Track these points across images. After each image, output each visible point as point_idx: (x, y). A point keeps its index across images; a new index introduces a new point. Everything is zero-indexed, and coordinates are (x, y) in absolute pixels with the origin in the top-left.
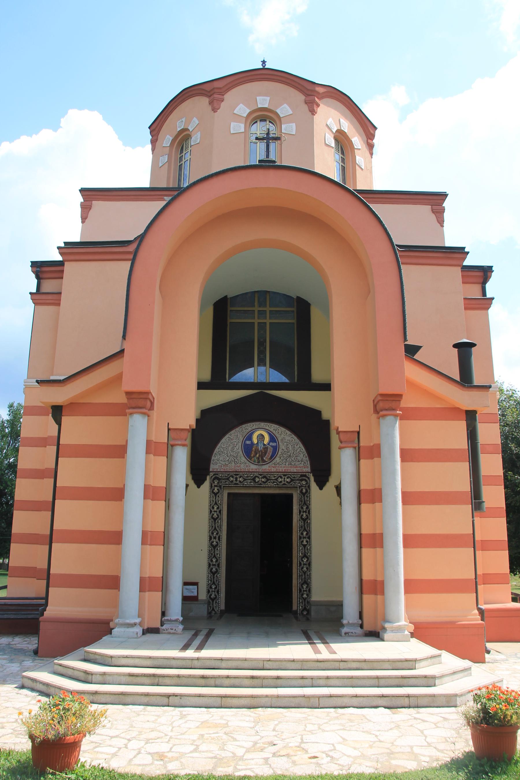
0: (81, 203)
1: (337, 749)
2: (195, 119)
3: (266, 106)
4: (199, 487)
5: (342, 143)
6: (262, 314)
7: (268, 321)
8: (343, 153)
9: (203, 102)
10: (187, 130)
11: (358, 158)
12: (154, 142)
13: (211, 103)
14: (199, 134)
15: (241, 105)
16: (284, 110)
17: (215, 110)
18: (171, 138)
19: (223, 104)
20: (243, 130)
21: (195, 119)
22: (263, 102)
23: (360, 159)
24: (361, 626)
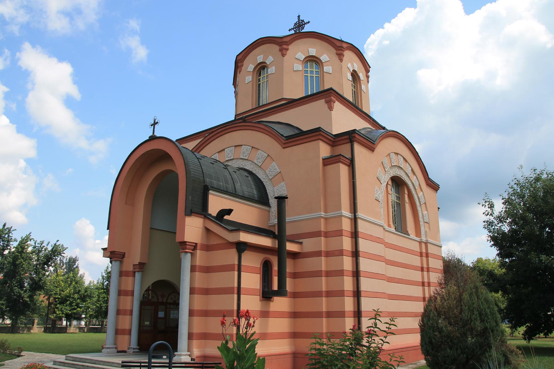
1: (418, 243)
2: (270, 57)
3: (314, 55)
5: (354, 75)
6: (312, 72)
7: (314, 75)
10: (265, 63)
11: (362, 86)
13: (281, 50)
16: (324, 58)
17: (283, 55)
18: (253, 67)
19: (288, 52)
21: (270, 57)
22: (313, 52)
24: (116, 348)
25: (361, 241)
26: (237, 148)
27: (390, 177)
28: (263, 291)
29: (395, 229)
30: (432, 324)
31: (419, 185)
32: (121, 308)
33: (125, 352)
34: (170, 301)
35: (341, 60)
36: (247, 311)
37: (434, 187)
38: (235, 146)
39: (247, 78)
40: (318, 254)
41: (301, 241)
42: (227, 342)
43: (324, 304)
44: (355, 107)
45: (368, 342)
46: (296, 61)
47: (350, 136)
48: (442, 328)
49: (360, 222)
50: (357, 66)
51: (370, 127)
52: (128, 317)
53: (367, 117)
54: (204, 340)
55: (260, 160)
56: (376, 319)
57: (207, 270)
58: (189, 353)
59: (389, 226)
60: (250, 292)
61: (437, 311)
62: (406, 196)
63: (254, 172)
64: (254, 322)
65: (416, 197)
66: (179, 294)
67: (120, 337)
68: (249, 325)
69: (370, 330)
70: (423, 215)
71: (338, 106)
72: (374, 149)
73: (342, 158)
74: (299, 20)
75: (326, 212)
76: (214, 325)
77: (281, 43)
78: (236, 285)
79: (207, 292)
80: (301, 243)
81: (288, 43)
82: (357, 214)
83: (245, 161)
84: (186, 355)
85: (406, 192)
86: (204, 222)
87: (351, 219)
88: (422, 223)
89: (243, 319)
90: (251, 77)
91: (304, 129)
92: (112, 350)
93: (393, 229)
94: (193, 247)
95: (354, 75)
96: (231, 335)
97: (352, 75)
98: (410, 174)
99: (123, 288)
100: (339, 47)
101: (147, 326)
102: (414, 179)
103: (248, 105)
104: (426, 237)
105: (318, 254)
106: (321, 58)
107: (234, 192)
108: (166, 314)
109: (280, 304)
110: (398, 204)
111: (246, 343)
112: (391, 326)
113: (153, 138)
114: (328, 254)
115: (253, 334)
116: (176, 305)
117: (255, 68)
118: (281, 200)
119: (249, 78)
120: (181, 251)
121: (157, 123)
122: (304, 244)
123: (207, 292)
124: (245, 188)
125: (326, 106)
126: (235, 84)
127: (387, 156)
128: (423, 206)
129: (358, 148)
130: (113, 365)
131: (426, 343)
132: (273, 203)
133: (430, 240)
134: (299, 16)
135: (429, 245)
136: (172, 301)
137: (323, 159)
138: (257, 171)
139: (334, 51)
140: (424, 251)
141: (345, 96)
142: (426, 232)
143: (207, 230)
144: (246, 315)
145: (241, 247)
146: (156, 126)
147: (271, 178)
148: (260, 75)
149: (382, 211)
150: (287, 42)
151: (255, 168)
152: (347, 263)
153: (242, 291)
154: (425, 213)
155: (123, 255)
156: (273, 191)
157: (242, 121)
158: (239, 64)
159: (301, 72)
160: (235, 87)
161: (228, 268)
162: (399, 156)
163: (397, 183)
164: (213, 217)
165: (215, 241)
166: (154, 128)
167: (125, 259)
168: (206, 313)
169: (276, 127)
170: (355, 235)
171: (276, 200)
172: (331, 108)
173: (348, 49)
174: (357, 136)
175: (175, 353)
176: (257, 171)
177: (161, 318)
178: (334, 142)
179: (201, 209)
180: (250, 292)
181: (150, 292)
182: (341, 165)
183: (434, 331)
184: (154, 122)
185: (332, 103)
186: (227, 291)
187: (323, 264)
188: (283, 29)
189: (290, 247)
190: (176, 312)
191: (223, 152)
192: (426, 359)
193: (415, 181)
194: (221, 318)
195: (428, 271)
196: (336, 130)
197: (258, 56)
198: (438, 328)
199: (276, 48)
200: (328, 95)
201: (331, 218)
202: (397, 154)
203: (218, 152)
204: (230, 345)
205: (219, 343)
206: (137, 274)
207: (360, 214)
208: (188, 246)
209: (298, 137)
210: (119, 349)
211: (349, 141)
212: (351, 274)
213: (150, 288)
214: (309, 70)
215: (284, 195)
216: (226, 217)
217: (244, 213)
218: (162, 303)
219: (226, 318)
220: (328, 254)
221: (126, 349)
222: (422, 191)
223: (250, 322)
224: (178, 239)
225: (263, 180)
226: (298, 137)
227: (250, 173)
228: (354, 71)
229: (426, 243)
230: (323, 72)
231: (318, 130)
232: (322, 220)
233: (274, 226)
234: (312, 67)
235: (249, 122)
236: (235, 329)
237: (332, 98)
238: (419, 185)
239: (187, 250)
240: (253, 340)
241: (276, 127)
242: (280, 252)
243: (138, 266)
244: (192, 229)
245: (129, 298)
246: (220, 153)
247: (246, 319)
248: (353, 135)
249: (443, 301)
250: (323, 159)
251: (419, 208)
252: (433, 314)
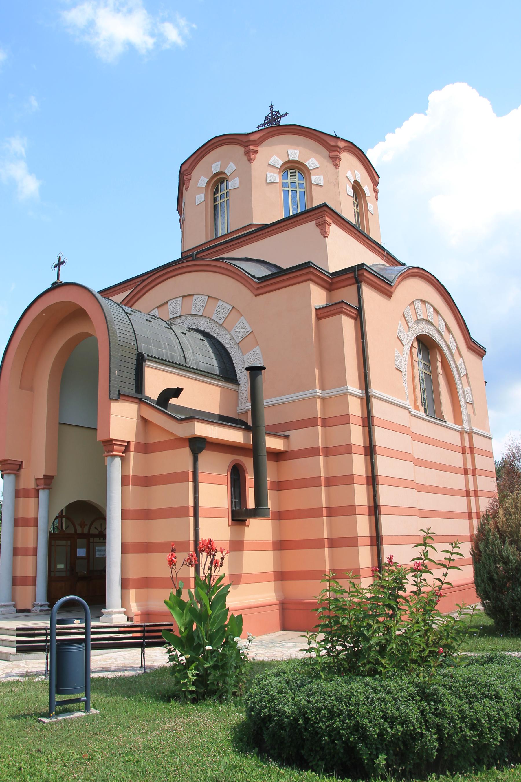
1: (459, 434)
3: (297, 159)
4: (183, 389)
5: (357, 187)
6: (294, 184)
7: (298, 189)
10: (224, 173)
11: (369, 204)
14: (237, 179)
16: (312, 162)
17: (250, 160)
18: (206, 180)
19: (258, 156)
21: (231, 164)
22: (295, 154)
23: (370, 206)
24: (14, 606)
25: (378, 432)
26: (186, 299)
27: (415, 335)
28: (233, 512)
29: (425, 412)
30: (492, 551)
31: (457, 348)
32: (19, 545)
33: (28, 611)
34: (93, 531)
35: (337, 166)
36: (210, 541)
37: (478, 351)
38: (183, 297)
39: (197, 196)
40: (313, 452)
41: (286, 433)
42: (179, 593)
43: (324, 528)
44: (359, 232)
45: (416, 584)
46: (270, 169)
47: (356, 275)
48: (508, 557)
49: (374, 402)
50: (360, 175)
51: (383, 262)
52: (30, 559)
53: (377, 248)
54: (145, 589)
55: (222, 316)
56: (425, 545)
57: (146, 481)
58: (124, 609)
59: (417, 408)
60: (214, 513)
61: (498, 531)
62: (439, 364)
63: (213, 334)
64: (223, 559)
65: (453, 365)
66: (105, 519)
67: (19, 588)
68: (214, 563)
69: (419, 564)
70: (464, 392)
71: (334, 230)
72: (392, 293)
74: (272, 112)
75: (322, 388)
76: (158, 565)
77: (245, 143)
78: (191, 503)
79: (146, 515)
80: (287, 437)
81: (258, 143)
82: (369, 390)
83: (199, 319)
84: (119, 613)
85: (439, 359)
86: (139, 408)
87: (361, 398)
88: (462, 404)
89: (205, 554)
90: (203, 195)
91: (285, 267)
92: (8, 609)
93: (422, 414)
94: (124, 448)
95: (357, 187)
96: (186, 581)
97: (353, 188)
98: (444, 332)
99: (20, 515)
100: (332, 146)
101: (60, 571)
102: (449, 339)
103: (200, 237)
104: (470, 424)
105: (313, 452)
106: (307, 164)
107: (184, 364)
108: (88, 552)
109: (259, 529)
110: (428, 377)
111: (213, 592)
112: (454, 557)
113: (57, 286)
114: (328, 452)
115: (221, 578)
116: (102, 537)
117: (209, 182)
118: (255, 371)
119: (200, 198)
120: (106, 454)
121: (63, 262)
122: (291, 437)
123: (146, 515)
124: (200, 358)
125: (318, 230)
126: (180, 208)
127: (410, 305)
128: (464, 379)
129: (367, 292)
130: (8, 632)
131: (483, 581)
132: (243, 377)
133: (475, 429)
134: (271, 106)
135: (473, 435)
136: (97, 532)
137: (316, 310)
138: (217, 331)
139: (326, 152)
140: (467, 444)
141: (345, 215)
142: (469, 417)
143: (144, 421)
144: (209, 548)
145: (198, 445)
146: (62, 266)
147: (238, 341)
148: (216, 192)
149: (407, 386)
150: (255, 141)
151: (214, 328)
152: (359, 465)
153: (201, 512)
154: (467, 388)
155: (20, 466)
156: (241, 361)
157: (191, 260)
158: (185, 177)
159: (278, 185)
160: (180, 213)
161: (178, 478)
162: (428, 306)
163: (426, 345)
164: (153, 401)
165: (156, 438)
166: (59, 270)
167: (23, 472)
168: (146, 548)
169: (243, 265)
170: (368, 422)
171: (248, 373)
172: (325, 234)
173: (345, 149)
174: (366, 274)
175: (103, 611)
176: (217, 331)
177: (82, 558)
178: (331, 284)
179: (137, 392)
180: (214, 513)
181: (64, 519)
182: (344, 318)
183: (495, 562)
184: (59, 261)
185: (327, 226)
186: (180, 512)
187: (321, 466)
188: (249, 123)
189: (272, 443)
190: (103, 548)
191: (165, 306)
192: (483, 605)
193: (451, 342)
194: (168, 555)
195: (474, 474)
196: (334, 266)
197: (213, 164)
198: (502, 557)
199: (240, 150)
200: (320, 214)
202: (424, 302)
203: (158, 307)
204: (185, 597)
205: (167, 593)
206: (41, 493)
207: (374, 390)
208: (115, 447)
209: (279, 277)
210: (20, 607)
211: (354, 281)
212: (364, 481)
213: (64, 514)
214: (289, 181)
215: (262, 365)
216: (173, 401)
217: (201, 395)
218: (82, 536)
219: (175, 554)
220: (328, 452)
221: (29, 606)
222: (461, 356)
223: (216, 558)
224: (101, 436)
225: (226, 345)
226: (279, 277)
227: (207, 335)
228: (356, 182)
229: (470, 434)
230: (311, 184)
231: (307, 265)
232: (318, 401)
233: (246, 413)
234: (293, 177)
235: (203, 260)
236: (192, 570)
237: (327, 218)
238: (457, 348)
239: (114, 453)
240: (221, 586)
241: (243, 265)
242: (255, 450)
243: (43, 481)
244: (122, 420)
245: (32, 529)
246: (161, 309)
247: (209, 554)
248: (361, 272)
249: (508, 516)
250: (316, 310)
251: (458, 382)
252: (493, 536)
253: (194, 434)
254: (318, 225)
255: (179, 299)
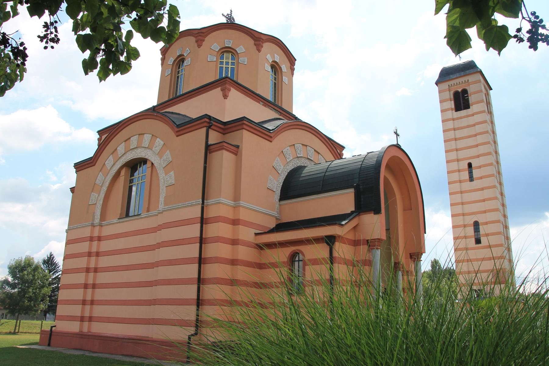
0: (122, 74)
3: (230, 46)
5: (275, 67)
8: (275, 74)
9: (192, 39)
12: (163, 60)
13: (197, 41)
15: (215, 44)
16: (240, 49)
17: (199, 46)
19: (204, 43)
20: (215, 60)
23: (285, 79)
35: (259, 51)
50: (279, 57)
71: (234, 93)
73: (225, 144)
97: (272, 67)
148: (179, 68)
172: (225, 97)
201: (212, 204)
214: (224, 61)
230: (238, 63)
253: (287, 262)
254: (222, 90)
255: (136, 137)
